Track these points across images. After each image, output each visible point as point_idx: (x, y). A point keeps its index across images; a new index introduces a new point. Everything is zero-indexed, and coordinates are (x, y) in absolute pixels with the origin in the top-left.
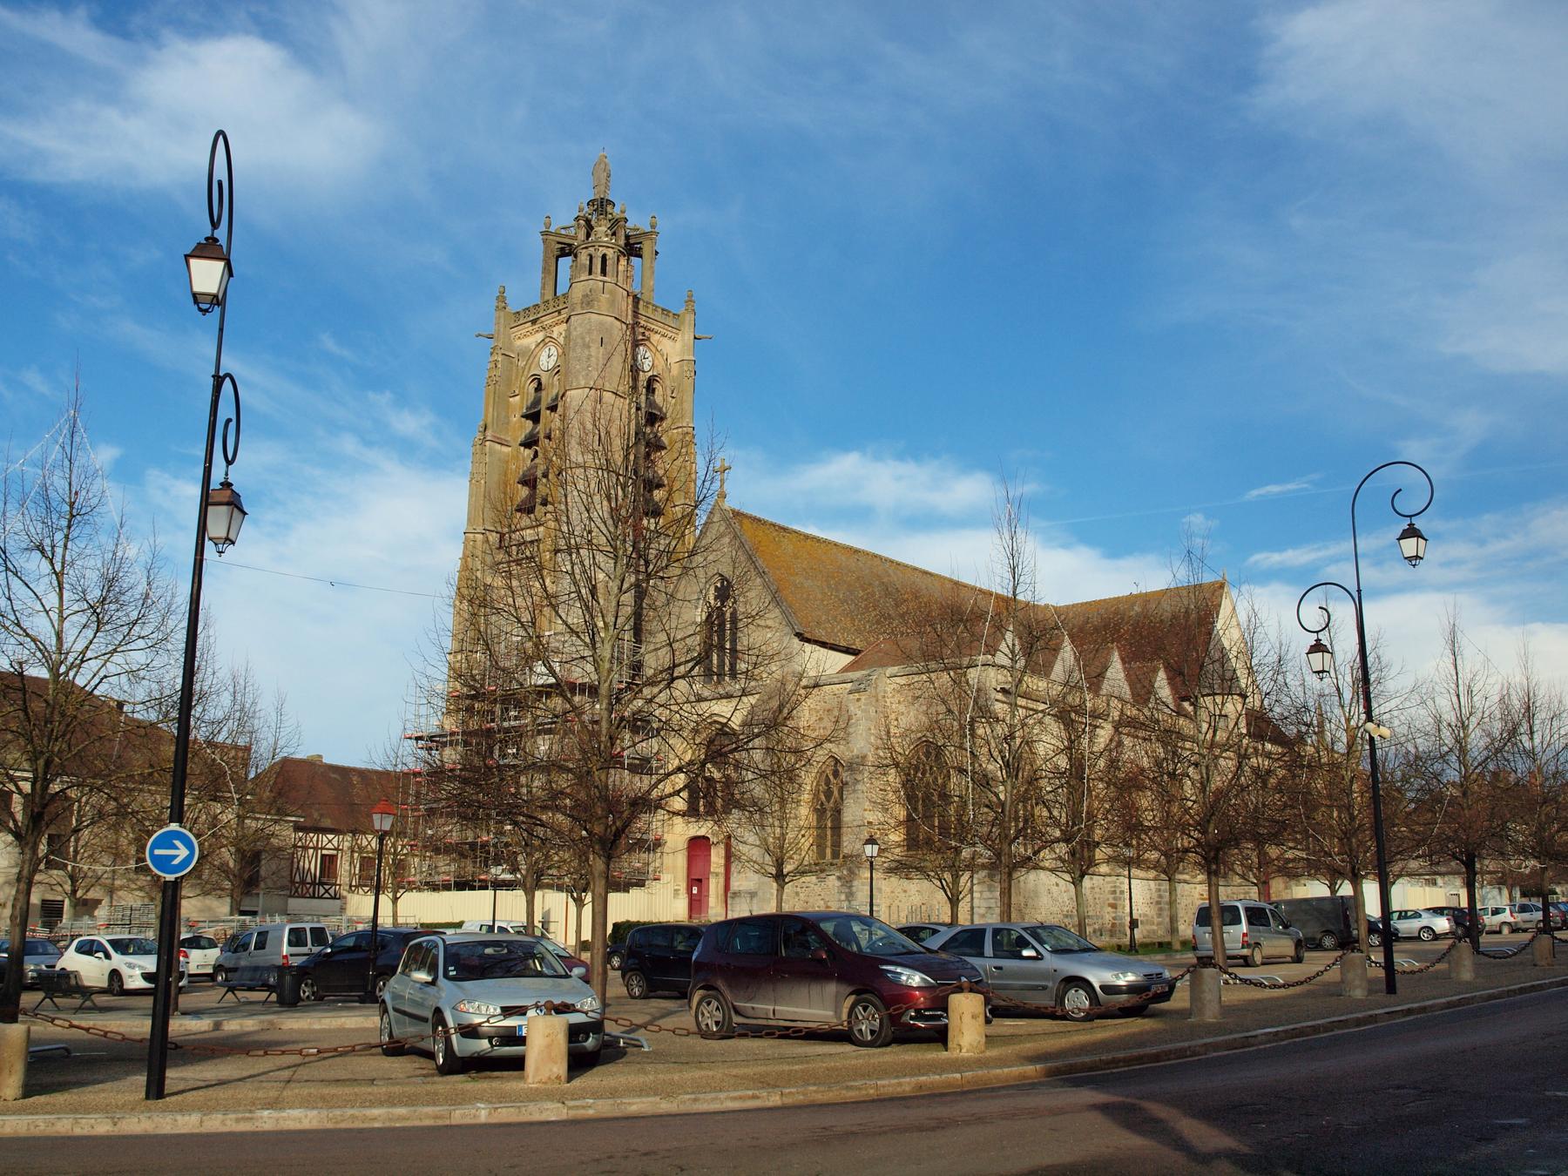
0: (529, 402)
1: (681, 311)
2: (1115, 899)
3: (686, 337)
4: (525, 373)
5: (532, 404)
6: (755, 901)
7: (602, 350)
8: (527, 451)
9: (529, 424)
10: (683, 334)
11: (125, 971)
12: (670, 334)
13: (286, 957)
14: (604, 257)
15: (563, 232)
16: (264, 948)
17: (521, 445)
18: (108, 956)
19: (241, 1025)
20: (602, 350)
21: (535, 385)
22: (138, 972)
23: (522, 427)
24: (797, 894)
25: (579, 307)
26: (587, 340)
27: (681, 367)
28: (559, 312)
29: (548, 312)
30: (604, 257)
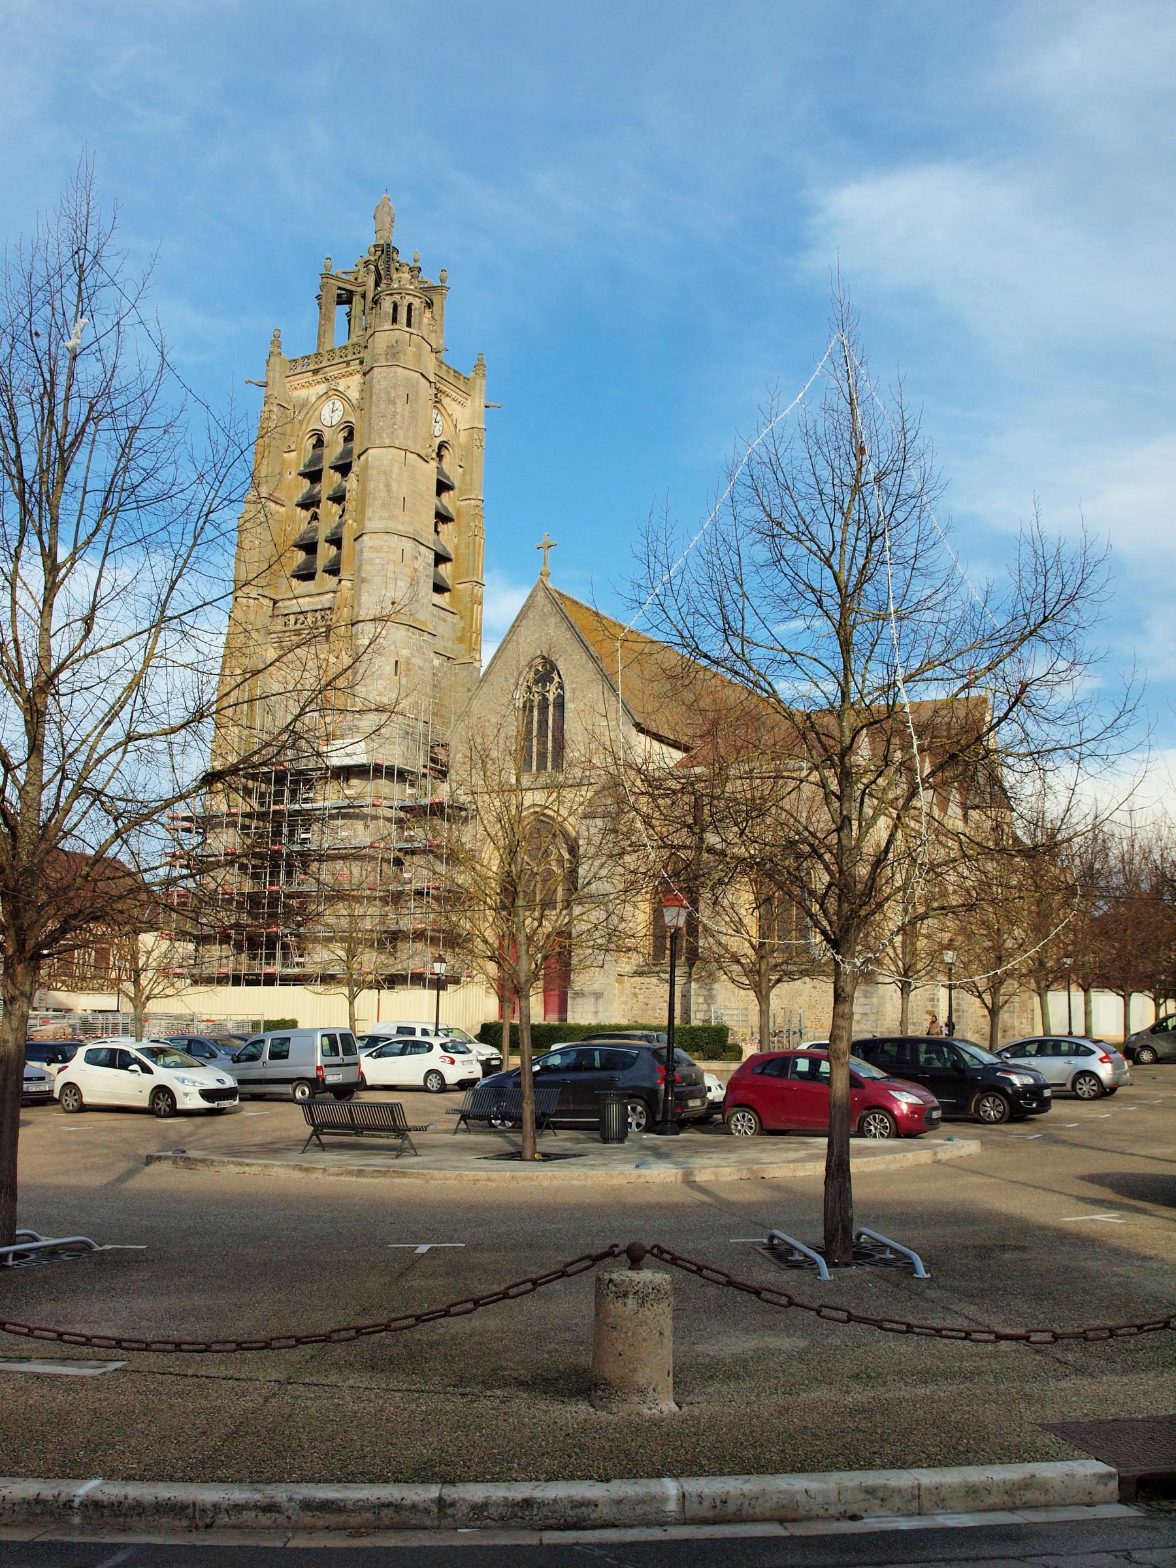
0: (307, 459)
1: (471, 375)
2: (933, 1006)
3: (477, 403)
4: (304, 427)
5: (310, 461)
6: (601, 1001)
7: (407, 407)
8: (304, 513)
9: (306, 483)
10: (473, 401)
11: (178, 1088)
12: (460, 399)
13: (319, 1068)
14: (410, 306)
15: (344, 276)
16: (286, 1057)
17: (298, 505)
18: (146, 1070)
19: (716, 1175)
20: (407, 407)
21: (313, 441)
22: (195, 1091)
23: (298, 486)
24: (635, 995)
25: (382, 358)
26: (393, 395)
27: (471, 436)
28: (348, 363)
29: (297, 371)
30: (410, 306)
